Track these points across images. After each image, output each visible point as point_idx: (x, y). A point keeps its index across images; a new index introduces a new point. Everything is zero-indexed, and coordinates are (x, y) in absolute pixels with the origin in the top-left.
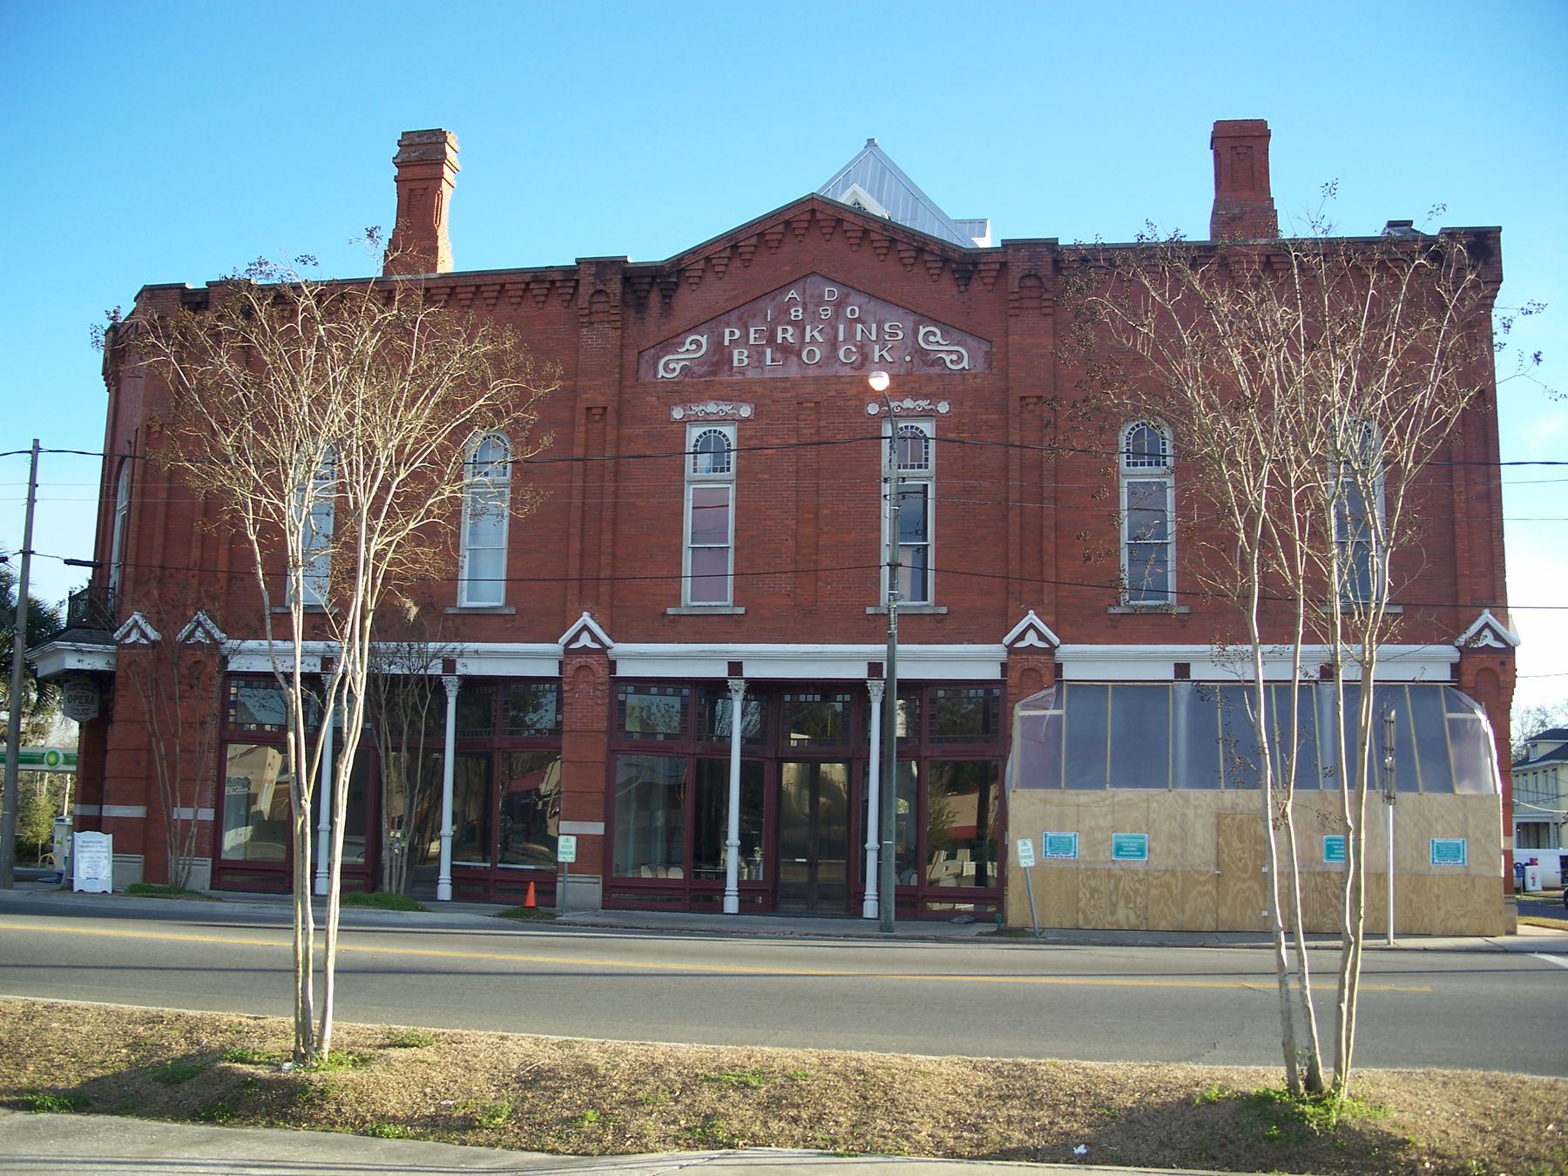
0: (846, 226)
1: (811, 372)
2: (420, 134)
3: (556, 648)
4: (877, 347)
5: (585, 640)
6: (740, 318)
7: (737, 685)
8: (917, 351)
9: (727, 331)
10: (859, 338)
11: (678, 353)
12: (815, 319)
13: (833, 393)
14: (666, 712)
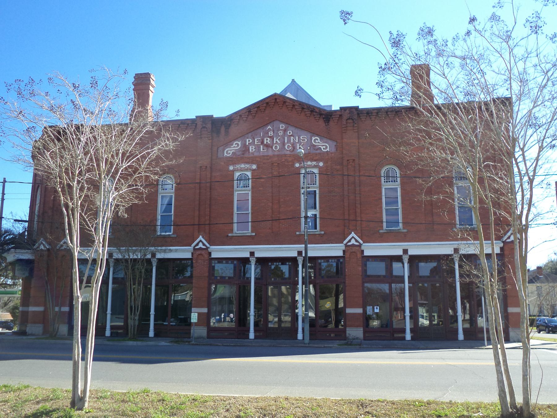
0: (287, 104)
1: (276, 153)
2: (141, 74)
3: (191, 248)
4: (298, 144)
5: (201, 245)
6: (252, 136)
7: (253, 261)
8: (312, 146)
9: (247, 140)
10: (292, 142)
11: (231, 148)
12: (278, 135)
13: (284, 160)
14: (227, 271)
